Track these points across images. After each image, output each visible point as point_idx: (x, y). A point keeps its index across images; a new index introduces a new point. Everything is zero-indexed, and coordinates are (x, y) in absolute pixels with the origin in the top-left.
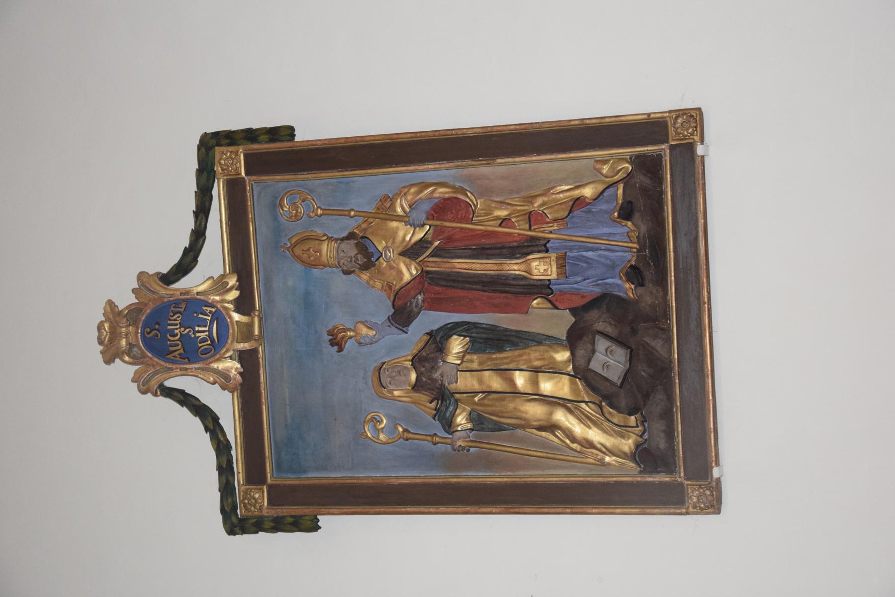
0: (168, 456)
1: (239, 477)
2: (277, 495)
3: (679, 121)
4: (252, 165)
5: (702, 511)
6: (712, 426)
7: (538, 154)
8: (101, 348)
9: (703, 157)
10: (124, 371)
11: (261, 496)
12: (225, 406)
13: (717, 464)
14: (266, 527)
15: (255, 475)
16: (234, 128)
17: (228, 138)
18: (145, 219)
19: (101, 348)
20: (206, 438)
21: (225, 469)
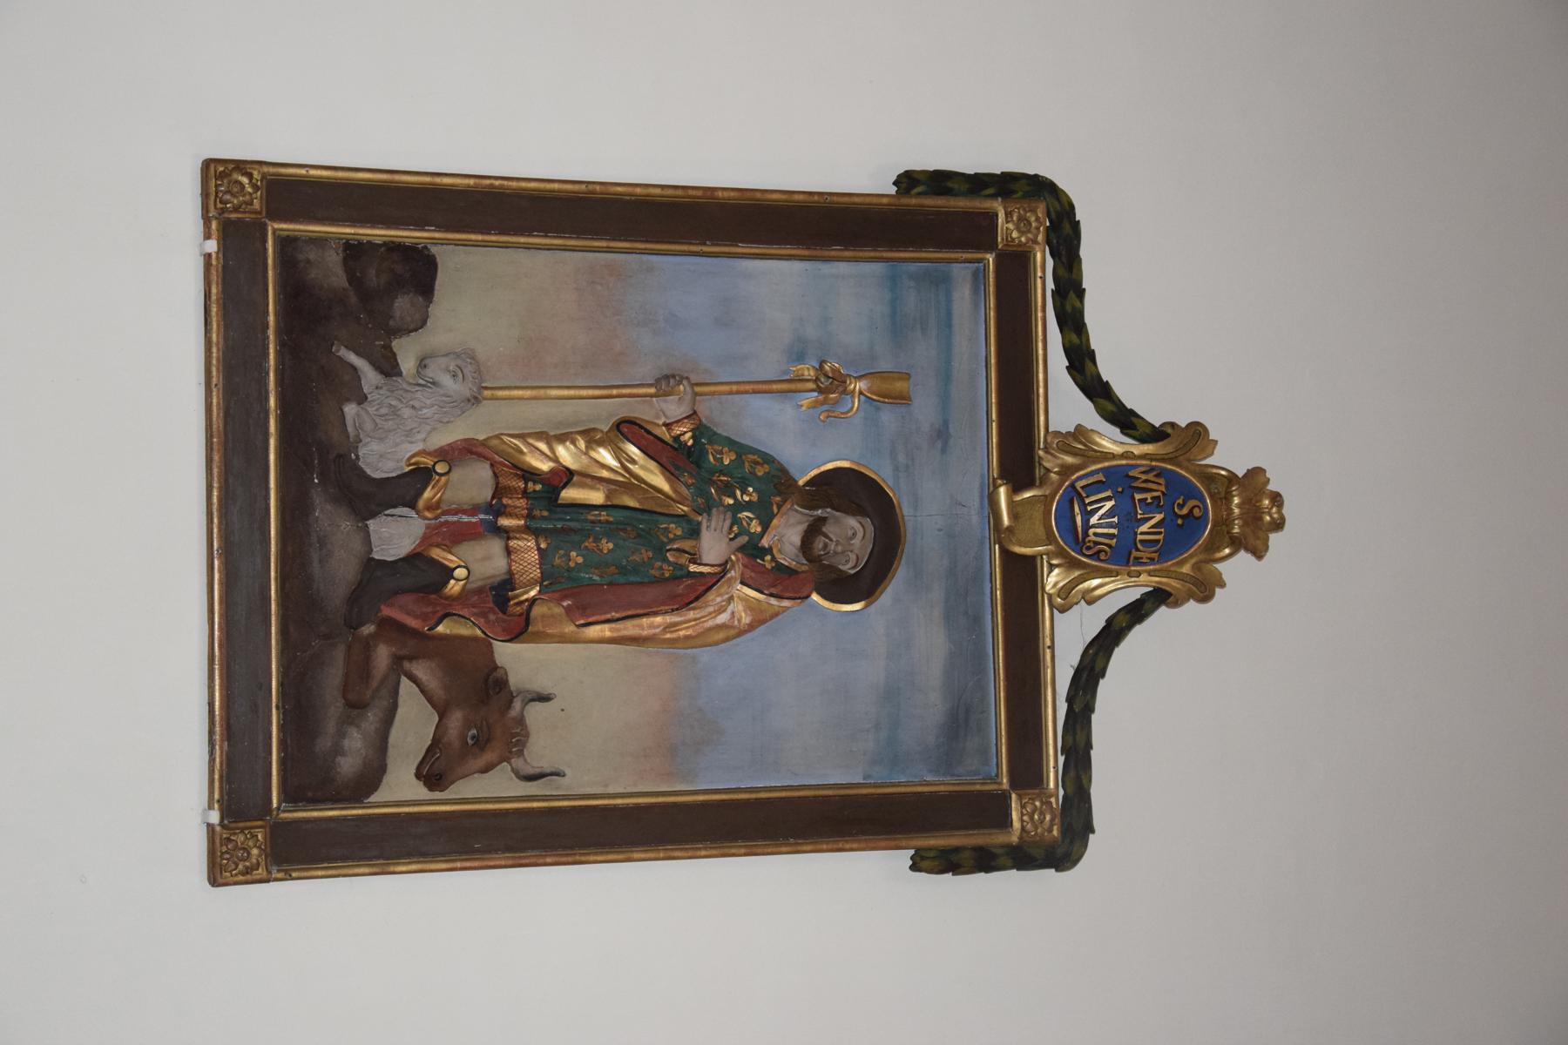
0: (1165, 328)
1: (1044, 265)
2: (978, 233)
3: (245, 180)
4: (988, 800)
5: (241, 166)
6: (216, 562)
7: (501, 233)
8: (1271, 487)
9: (210, 807)
10: (1229, 457)
11: (1006, 228)
12: (1063, 406)
13: (208, 257)
14: (967, 854)
15: (1015, 267)
16: (1013, 875)
17: (1024, 857)
18: (1176, 706)
19: (1271, 487)
20: (1098, 340)
21: (1070, 290)
